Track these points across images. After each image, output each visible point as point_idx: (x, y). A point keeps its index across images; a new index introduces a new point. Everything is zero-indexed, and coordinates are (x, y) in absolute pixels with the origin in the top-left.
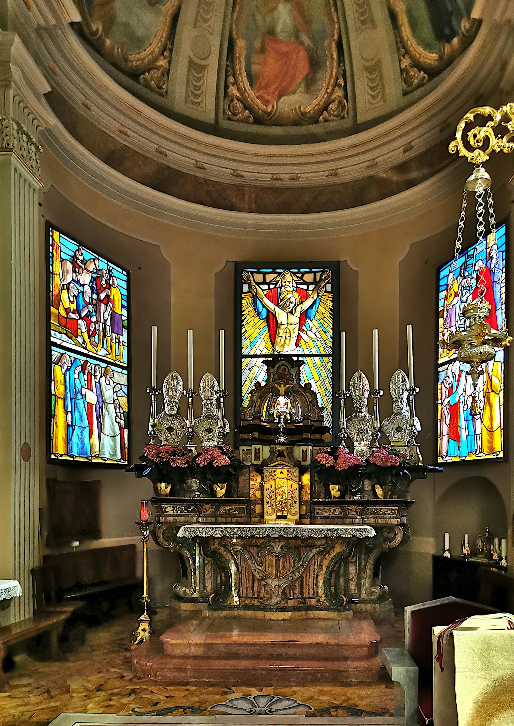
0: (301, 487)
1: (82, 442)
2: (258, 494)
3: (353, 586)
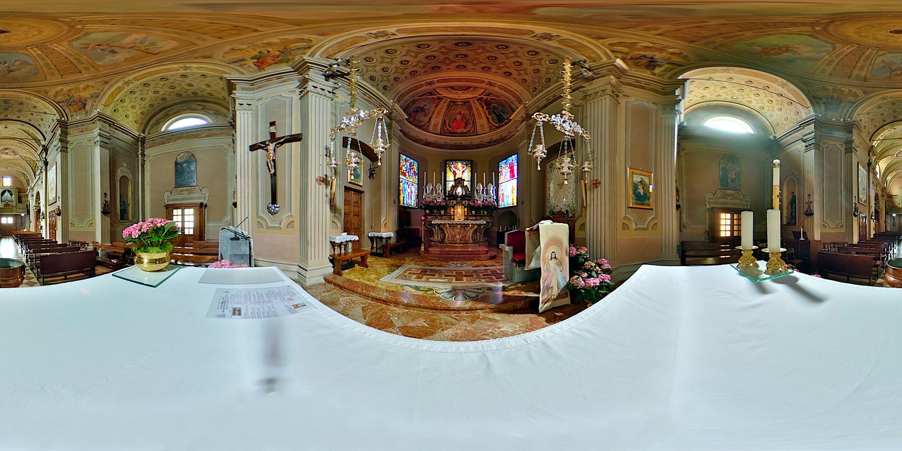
0: (465, 211)
1: (407, 201)
2: (453, 213)
3: (478, 238)
